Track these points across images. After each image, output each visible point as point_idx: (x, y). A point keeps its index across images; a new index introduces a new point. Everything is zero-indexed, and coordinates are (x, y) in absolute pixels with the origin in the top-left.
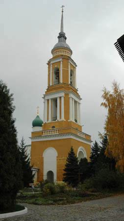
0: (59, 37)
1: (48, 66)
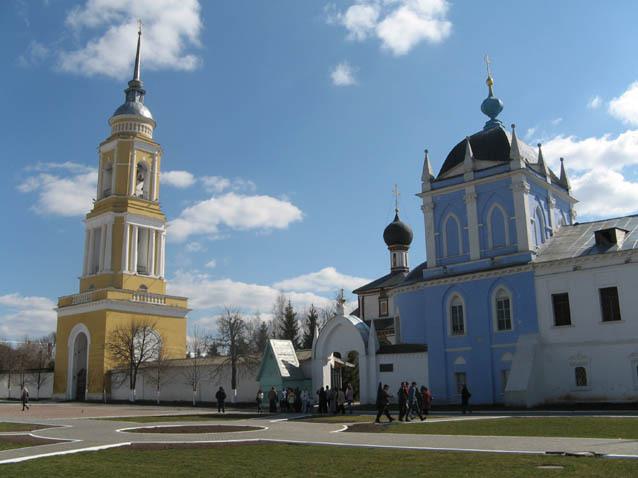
0: (127, 92)
1: (125, 95)
